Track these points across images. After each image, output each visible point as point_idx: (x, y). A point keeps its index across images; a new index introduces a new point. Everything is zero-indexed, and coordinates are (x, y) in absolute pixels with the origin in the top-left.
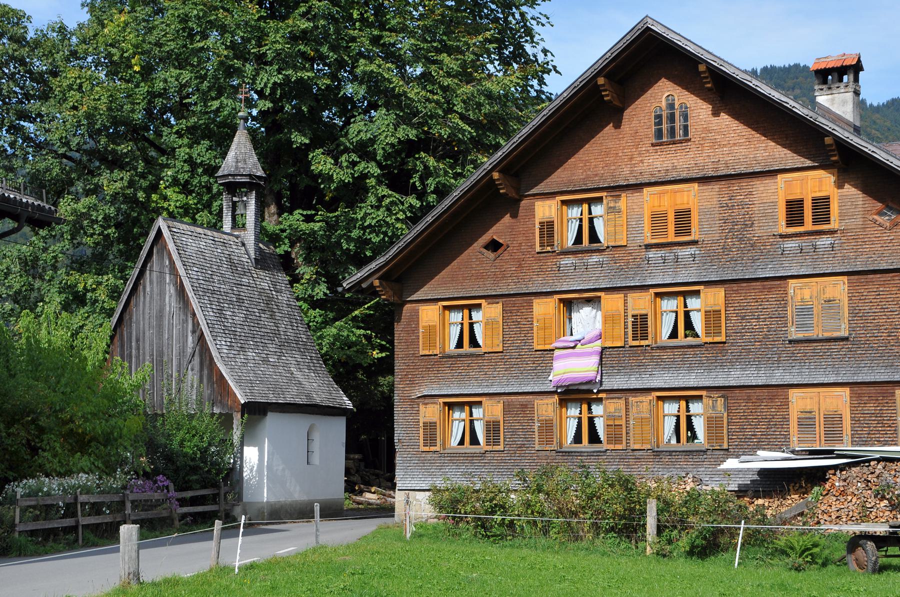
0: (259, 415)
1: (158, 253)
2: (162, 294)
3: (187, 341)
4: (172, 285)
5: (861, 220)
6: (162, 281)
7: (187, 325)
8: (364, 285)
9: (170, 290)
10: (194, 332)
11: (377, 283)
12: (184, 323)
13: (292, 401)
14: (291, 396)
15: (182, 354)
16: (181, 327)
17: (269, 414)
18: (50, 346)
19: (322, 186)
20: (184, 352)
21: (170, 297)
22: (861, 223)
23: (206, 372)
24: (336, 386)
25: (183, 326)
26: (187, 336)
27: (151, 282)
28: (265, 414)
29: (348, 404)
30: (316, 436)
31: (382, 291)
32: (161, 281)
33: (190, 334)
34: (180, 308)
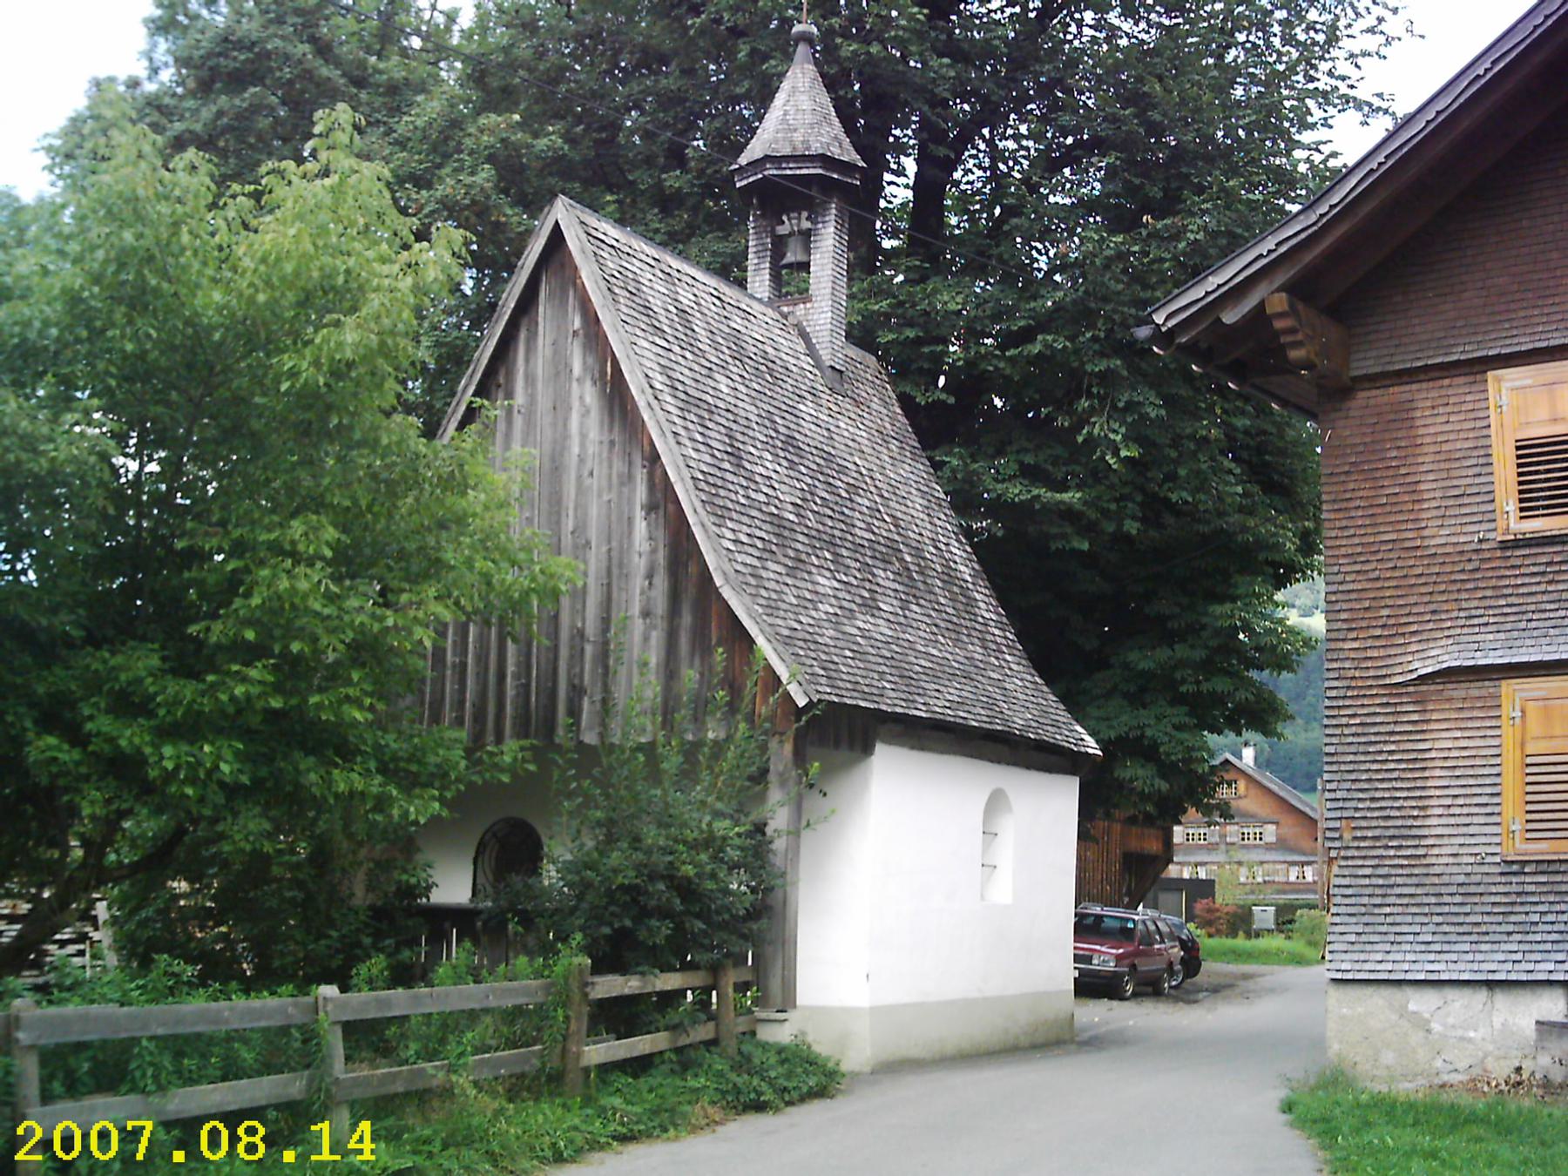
0: (851, 747)
1: (550, 296)
2: (560, 407)
3: (630, 533)
4: (588, 383)
5: (1423, 487)
6: (560, 369)
7: (633, 490)
8: (1230, 317)
9: (586, 396)
10: (651, 508)
11: (1279, 303)
12: (622, 484)
13: (950, 715)
14: (936, 703)
15: (615, 571)
16: (613, 496)
17: (881, 750)
18: (1325, 97)
19: (954, 18)
20: (621, 565)
21: (586, 413)
22: (1423, 487)
23: (687, 619)
24: (1045, 689)
25: (620, 493)
26: (630, 520)
27: (530, 380)
28: (867, 750)
29: (1092, 746)
30: (1008, 827)
31: (1292, 331)
32: (557, 374)
33: (639, 514)
34: (612, 443)
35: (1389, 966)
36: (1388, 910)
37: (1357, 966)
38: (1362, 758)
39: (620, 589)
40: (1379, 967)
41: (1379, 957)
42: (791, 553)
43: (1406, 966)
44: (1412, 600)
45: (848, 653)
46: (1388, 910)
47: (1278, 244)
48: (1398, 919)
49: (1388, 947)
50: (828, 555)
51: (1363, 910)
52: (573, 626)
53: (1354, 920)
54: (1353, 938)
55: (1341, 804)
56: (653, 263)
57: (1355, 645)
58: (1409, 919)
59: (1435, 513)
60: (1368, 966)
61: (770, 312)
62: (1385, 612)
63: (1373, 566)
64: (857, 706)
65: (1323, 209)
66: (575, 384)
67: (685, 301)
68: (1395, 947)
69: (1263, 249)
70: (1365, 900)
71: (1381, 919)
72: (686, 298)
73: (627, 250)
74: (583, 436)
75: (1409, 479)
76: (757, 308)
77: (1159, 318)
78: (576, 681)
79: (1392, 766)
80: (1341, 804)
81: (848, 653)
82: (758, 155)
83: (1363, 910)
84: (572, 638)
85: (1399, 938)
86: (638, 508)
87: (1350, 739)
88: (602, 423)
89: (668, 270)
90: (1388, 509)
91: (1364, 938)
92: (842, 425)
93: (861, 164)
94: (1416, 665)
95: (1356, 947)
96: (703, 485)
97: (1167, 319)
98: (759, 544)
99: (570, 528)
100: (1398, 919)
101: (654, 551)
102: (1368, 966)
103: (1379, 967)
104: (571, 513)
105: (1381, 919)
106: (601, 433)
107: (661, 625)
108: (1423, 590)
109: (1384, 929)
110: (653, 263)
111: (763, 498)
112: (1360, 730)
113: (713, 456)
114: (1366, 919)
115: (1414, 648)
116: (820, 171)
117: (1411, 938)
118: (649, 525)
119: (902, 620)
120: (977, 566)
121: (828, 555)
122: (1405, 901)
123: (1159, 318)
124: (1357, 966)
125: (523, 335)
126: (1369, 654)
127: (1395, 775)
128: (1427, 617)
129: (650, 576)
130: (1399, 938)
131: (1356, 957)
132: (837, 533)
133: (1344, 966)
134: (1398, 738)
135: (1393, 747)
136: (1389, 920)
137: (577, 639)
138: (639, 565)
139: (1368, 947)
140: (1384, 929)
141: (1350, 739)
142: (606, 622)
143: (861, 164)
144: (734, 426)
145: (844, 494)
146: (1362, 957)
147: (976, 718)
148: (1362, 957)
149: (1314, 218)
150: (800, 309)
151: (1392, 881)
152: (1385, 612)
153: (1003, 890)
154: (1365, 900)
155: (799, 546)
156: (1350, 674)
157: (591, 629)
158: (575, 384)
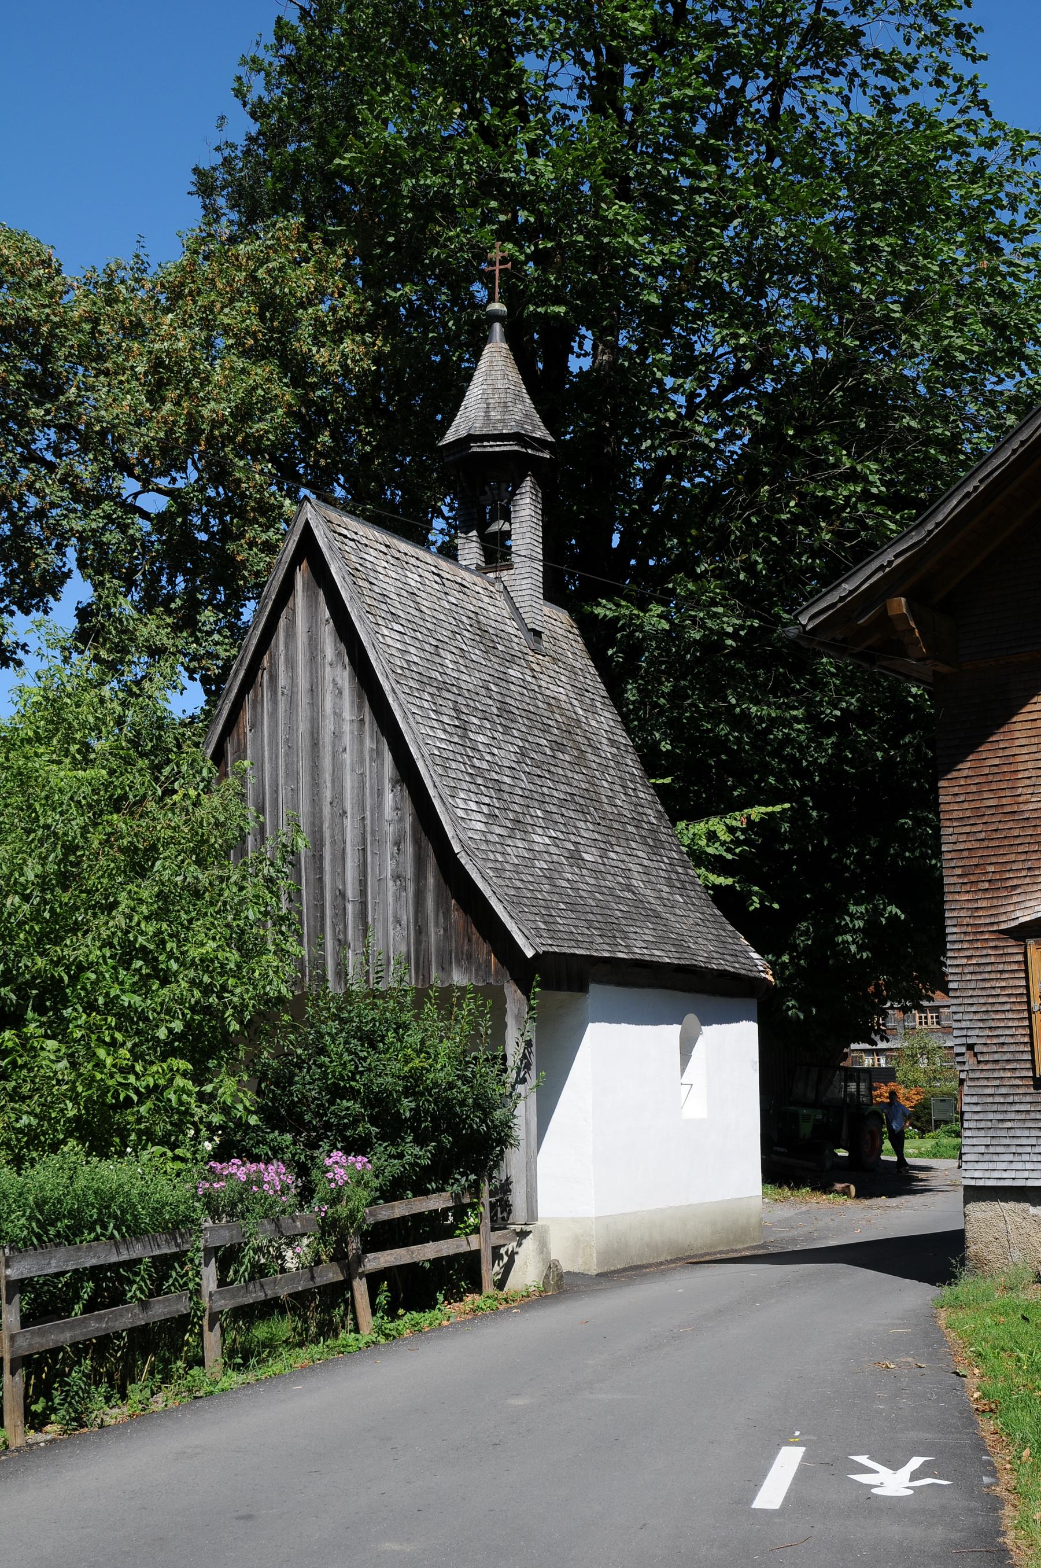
17: (594, 988)
28: (583, 989)
33: (387, 786)
34: (362, 721)
35: (1013, 1175)
36: (1009, 1125)
37: (987, 1175)
38: (980, 993)
39: (373, 854)
40: (1005, 1175)
41: (1004, 1166)
42: (511, 815)
43: (1026, 1174)
44: (1012, 858)
45: (562, 906)
46: (1009, 1125)
47: (896, 556)
48: (1018, 1133)
49: (1010, 1157)
50: (539, 813)
51: (989, 1124)
52: (334, 888)
53: (982, 1133)
54: (983, 1149)
55: (964, 1033)
56: (384, 549)
57: (966, 897)
58: (1026, 1133)
59: (1028, 782)
60: (996, 1175)
61: (477, 580)
62: (991, 868)
63: (979, 828)
64: (575, 955)
65: (930, 526)
66: (328, 669)
67: (413, 583)
68: (1017, 1158)
69: (884, 560)
70: (991, 1116)
71: (1003, 1133)
72: (413, 579)
73: (365, 541)
74: (338, 715)
75: (1007, 753)
76: (469, 578)
77: (803, 620)
78: (341, 937)
79: (1004, 999)
80: (964, 1033)
81: (562, 906)
82: (463, 433)
83: (989, 1124)
84: (334, 898)
85: (1020, 1150)
86: (386, 781)
87: (969, 977)
88: (353, 702)
89: (398, 555)
90: (990, 778)
91: (992, 1150)
92: (543, 684)
93: (550, 439)
94: (1018, 914)
95: (987, 1157)
96: (438, 760)
97: (811, 619)
98: (485, 809)
99: (329, 800)
100: (1018, 1133)
101: (401, 820)
102: (996, 1175)
103: (1005, 1175)
104: (329, 785)
105: (1003, 1133)
106: (352, 714)
107: (411, 887)
108: (1021, 849)
109: (1007, 1141)
110: (384, 549)
111: (485, 766)
112: (977, 969)
113: (445, 731)
114: (991, 1133)
115: (1015, 899)
116: (516, 448)
117: (1029, 1149)
118: (395, 796)
119: (602, 868)
120: (660, 807)
121: (539, 813)
122: (1023, 1116)
123: (803, 620)
124: (987, 1175)
125: (282, 623)
126: (980, 904)
127: (1007, 1007)
128: (1024, 873)
129: (397, 844)
130: (1020, 1150)
131: (985, 1166)
132: (545, 790)
133: (977, 1174)
134: (1007, 976)
135: (1003, 984)
136: (1011, 1133)
137: (339, 898)
138: (390, 831)
139: (995, 1158)
140: (1007, 1141)
141: (969, 977)
142: (363, 883)
143: (550, 439)
144: (460, 700)
145: (549, 752)
146: (991, 1166)
147: (664, 956)
148: (991, 1166)
149: (924, 534)
150: (505, 575)
151: (1011, 1099)
152: (991, 868)
153: (696, 1108)
154: (991, 1116)
155: (517, 808)
156: (966, 921)
157: (351, 891)
158: (328, 669)
